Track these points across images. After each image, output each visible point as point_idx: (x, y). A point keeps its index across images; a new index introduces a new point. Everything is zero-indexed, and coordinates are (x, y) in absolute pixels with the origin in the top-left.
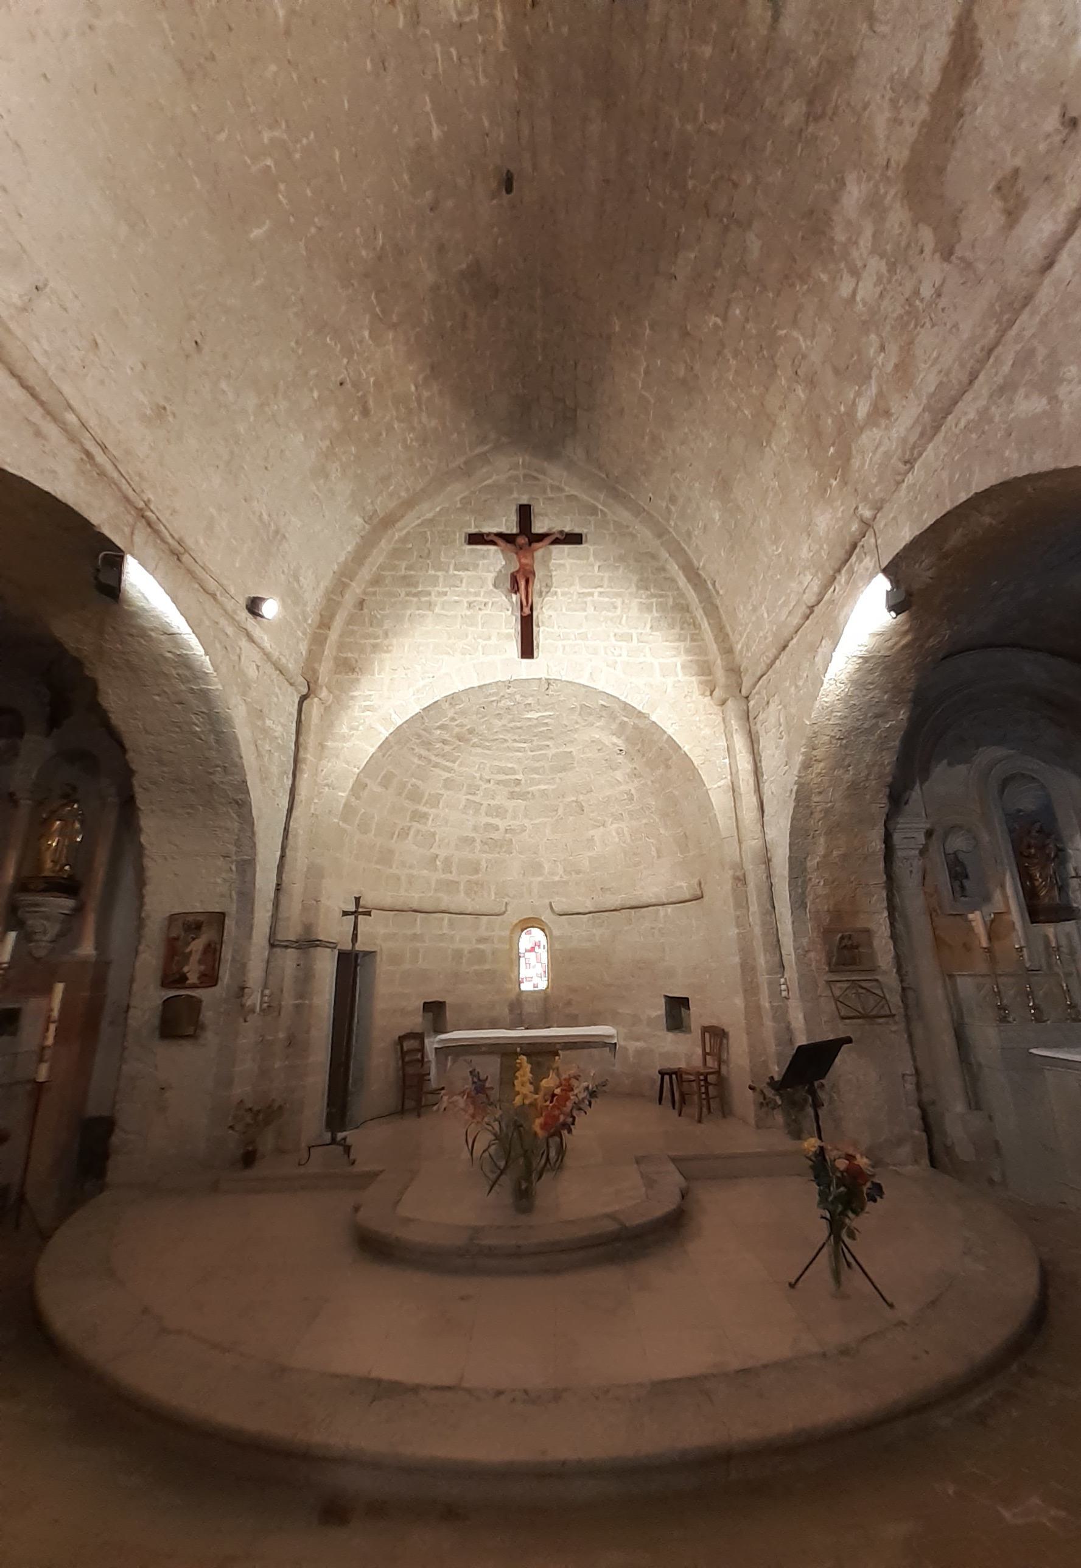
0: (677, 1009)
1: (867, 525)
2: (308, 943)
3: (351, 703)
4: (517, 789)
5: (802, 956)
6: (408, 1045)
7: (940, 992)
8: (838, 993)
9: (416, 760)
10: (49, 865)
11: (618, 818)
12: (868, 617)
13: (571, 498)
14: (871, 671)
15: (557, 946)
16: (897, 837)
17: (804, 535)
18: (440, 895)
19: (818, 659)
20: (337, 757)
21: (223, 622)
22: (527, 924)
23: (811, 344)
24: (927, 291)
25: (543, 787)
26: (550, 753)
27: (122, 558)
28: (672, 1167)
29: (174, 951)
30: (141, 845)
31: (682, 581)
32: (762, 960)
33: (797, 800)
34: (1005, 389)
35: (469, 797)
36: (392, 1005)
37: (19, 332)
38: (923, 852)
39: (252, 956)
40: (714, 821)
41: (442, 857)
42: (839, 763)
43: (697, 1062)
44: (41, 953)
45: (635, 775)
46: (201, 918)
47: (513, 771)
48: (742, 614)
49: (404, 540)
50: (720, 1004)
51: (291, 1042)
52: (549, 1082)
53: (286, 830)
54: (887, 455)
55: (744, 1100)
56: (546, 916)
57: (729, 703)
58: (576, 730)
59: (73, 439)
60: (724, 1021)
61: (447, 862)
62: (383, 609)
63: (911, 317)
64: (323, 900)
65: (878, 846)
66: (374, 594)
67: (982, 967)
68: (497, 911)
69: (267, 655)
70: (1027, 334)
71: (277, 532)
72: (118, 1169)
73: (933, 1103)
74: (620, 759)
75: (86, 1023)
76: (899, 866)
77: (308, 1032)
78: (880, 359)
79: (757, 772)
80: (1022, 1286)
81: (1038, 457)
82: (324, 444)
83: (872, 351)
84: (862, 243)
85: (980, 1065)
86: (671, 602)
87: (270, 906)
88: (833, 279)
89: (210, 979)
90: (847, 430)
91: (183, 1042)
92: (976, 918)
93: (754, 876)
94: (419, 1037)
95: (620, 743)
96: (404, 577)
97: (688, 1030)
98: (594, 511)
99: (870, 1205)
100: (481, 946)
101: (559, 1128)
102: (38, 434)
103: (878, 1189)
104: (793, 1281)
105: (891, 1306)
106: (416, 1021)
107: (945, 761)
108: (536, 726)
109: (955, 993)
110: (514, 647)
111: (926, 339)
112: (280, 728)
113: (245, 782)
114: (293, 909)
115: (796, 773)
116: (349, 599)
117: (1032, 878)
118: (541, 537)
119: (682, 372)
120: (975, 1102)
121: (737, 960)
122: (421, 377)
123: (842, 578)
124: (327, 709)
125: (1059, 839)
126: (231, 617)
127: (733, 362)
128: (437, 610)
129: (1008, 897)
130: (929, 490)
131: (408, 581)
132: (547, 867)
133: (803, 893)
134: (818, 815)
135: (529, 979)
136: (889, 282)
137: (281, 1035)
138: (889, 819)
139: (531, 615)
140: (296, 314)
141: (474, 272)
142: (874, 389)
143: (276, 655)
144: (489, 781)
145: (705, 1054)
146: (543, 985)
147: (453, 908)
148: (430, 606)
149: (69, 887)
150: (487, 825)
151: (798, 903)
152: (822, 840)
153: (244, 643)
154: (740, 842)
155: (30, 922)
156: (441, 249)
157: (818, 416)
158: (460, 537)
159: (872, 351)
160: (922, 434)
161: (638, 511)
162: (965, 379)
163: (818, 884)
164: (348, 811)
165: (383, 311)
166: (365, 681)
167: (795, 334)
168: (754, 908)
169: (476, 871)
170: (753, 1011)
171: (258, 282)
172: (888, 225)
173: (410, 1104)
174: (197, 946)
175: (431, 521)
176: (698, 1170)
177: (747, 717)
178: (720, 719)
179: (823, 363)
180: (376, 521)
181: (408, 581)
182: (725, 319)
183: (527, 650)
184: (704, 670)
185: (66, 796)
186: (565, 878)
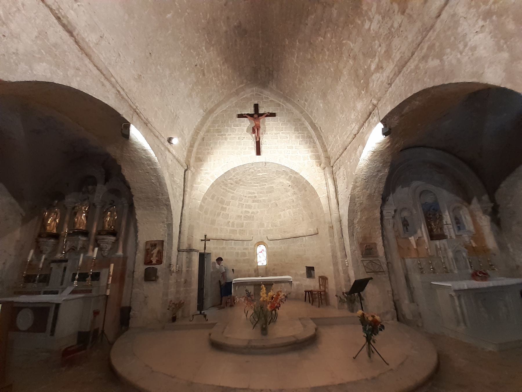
0: (310, 270)
1: (375, 106)
2: (190, 250)
4: (255, 199)
5: (353, 252)
7: (400, 264)
8: (365, 264)
9: (222, 190)
10: (107, 226)
11: (289, 208)
12: (376, 137)
13: (271, 101)
14: (376, 156)
15: (269, 251)
16: (384, 213)
17: (353, 110)
19: (358, 152)
21: (161, 146)
23: (354, 46)
24: (396, 25)
26: (266, 187)
27: (129, 125)
28: (311, 321)
29: (148, 253)
30: (136, 220)
31: (310, 128)
32: (339, 254)
33: (350, 200)
34: (425, 58)
37: (96, 52)
38: (393, 217)
40: (322, 208)
41: (231, 222)
42: (365, 188)
43: (317, 288)
44: (106, 254)
45: (295, 193)
47: (254, 193)
48: (330, 138)
49: (216, 117)
50: (324, 269)
51: (186, 282)
52: (271, 294)
53: (182, 213)
54: (382, 82)
55: (334, 300)
56: (266, 241)
57: (326, 168)
58: (275, 179)
59: (114, 86)
60: (326, 275)
61: (233, 225)
63: (390, 35)
64: (194, 237)
65: (378, 215)
67: (414, 255)
69: (174, 156)
70: (432, 38)
71: (176, 116)
72: (133, 323)
73: (398, 300)
74: (290, 188)
75: (121, 277)
76: (385, 222)
77: (191, 279)
78: (379, 49)
79: (336, 191)
80: (431, 360)
81: (436, 80)
82: (191, 86)
83: (376, 47)
84: (372, 10)
85: (414, 288)
86: (306, 135)
87: (177, 239)
88: (362, 23)
89: (159, 262)
90: (368, 74)
91: (152, 282)
92: (412, 239)
95: (290, 183)
97: (314, 277)
98: (279, 105)
99: (380, 332)
101: (275, 308)
102: (103, 85)
103: (383, 327)
104: (354, 356)
105: (388, 364)
107: (400, 186)
108: (262, 178)
109: (405, 264)
110: (254, 152)
111: (396, 42)
112: (179, 181)
113: (169, 198)
114: (185, 239)
115: (350, 191)
116: (199, 138)
117: (431, 225)
118: (262, 115)
119: (309, 57)
120: (412, 300)
122: (221, 62)
123: (366, 124)
124: (193, 174)
125: (441, 212)
126: (163, 144)
127: (327, 53)
128: (228, 140)
129: (423, 232)
130: (397, 93)
131: (218, 131)
132: (265, 224)
136: (382, 22)
137: (183, 280)
138: (382, 206)
140: (181, 43)
141: (239, 26)
142: (377, 60)
143: (177, 156)
145: (320, 285)
146: (265, 263)
147: (235, 238)
148: (226, 139)
149: (114, 233)
150: (245, 211)
151: (351, 235)
152: (359, 213)
153: (167, 152)
154: (331, 215)
155: (102, 245)
156: (228, 18)
157: (357, 70)
158: (235, 116)
159: (376, 47)
160: (395, 74)
161: (294, 105)
162: (410, 55)
164: (201, 207)
165: (209, 40)
167: (349, 42)
168: (336, 236)
169: (242, 226)
170: (337, 271)
171: (170, 32)
172: (382, 3)
174: (155, 251)
176: (321, 322)
177: (333, 173)
178: (323, 174)
179: (359, 51)
180: (207, 111)
181: (218, 131)
182: (324, 38)
183: (258, 153)
184: (318, 158)
185: (111, 204)
186: (272, 228)
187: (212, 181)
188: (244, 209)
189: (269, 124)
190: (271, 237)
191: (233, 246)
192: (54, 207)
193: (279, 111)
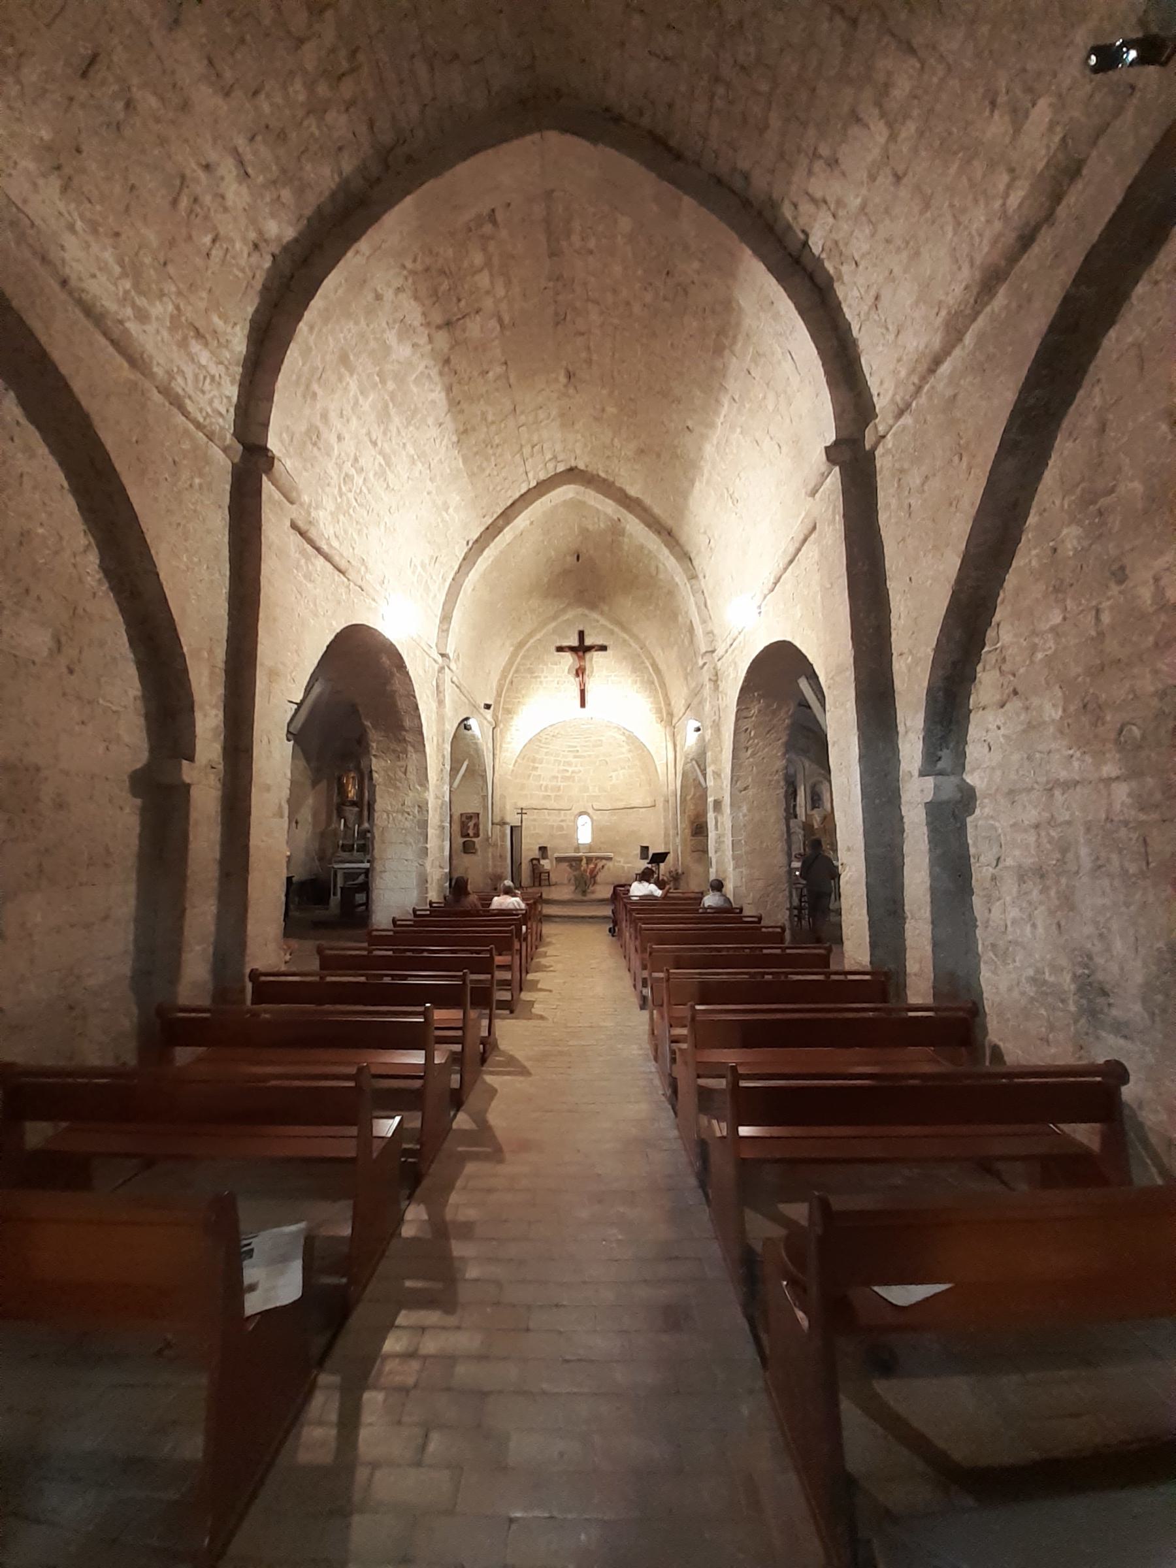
22: (581, 814)
32: (671, 832)
36: (529, 848)
39: (487, 827)
45: (630, 751)
56: (590, 811)
89: (477, 835)
98: (612, 632)
114: (496, 810)
131: (531, 671)
151: (683, 812)
158: (553, 649)
166: (515, 717)
181: (531, 671)
183: (583, 704)
184: (659, 711)
188: (562, 768)
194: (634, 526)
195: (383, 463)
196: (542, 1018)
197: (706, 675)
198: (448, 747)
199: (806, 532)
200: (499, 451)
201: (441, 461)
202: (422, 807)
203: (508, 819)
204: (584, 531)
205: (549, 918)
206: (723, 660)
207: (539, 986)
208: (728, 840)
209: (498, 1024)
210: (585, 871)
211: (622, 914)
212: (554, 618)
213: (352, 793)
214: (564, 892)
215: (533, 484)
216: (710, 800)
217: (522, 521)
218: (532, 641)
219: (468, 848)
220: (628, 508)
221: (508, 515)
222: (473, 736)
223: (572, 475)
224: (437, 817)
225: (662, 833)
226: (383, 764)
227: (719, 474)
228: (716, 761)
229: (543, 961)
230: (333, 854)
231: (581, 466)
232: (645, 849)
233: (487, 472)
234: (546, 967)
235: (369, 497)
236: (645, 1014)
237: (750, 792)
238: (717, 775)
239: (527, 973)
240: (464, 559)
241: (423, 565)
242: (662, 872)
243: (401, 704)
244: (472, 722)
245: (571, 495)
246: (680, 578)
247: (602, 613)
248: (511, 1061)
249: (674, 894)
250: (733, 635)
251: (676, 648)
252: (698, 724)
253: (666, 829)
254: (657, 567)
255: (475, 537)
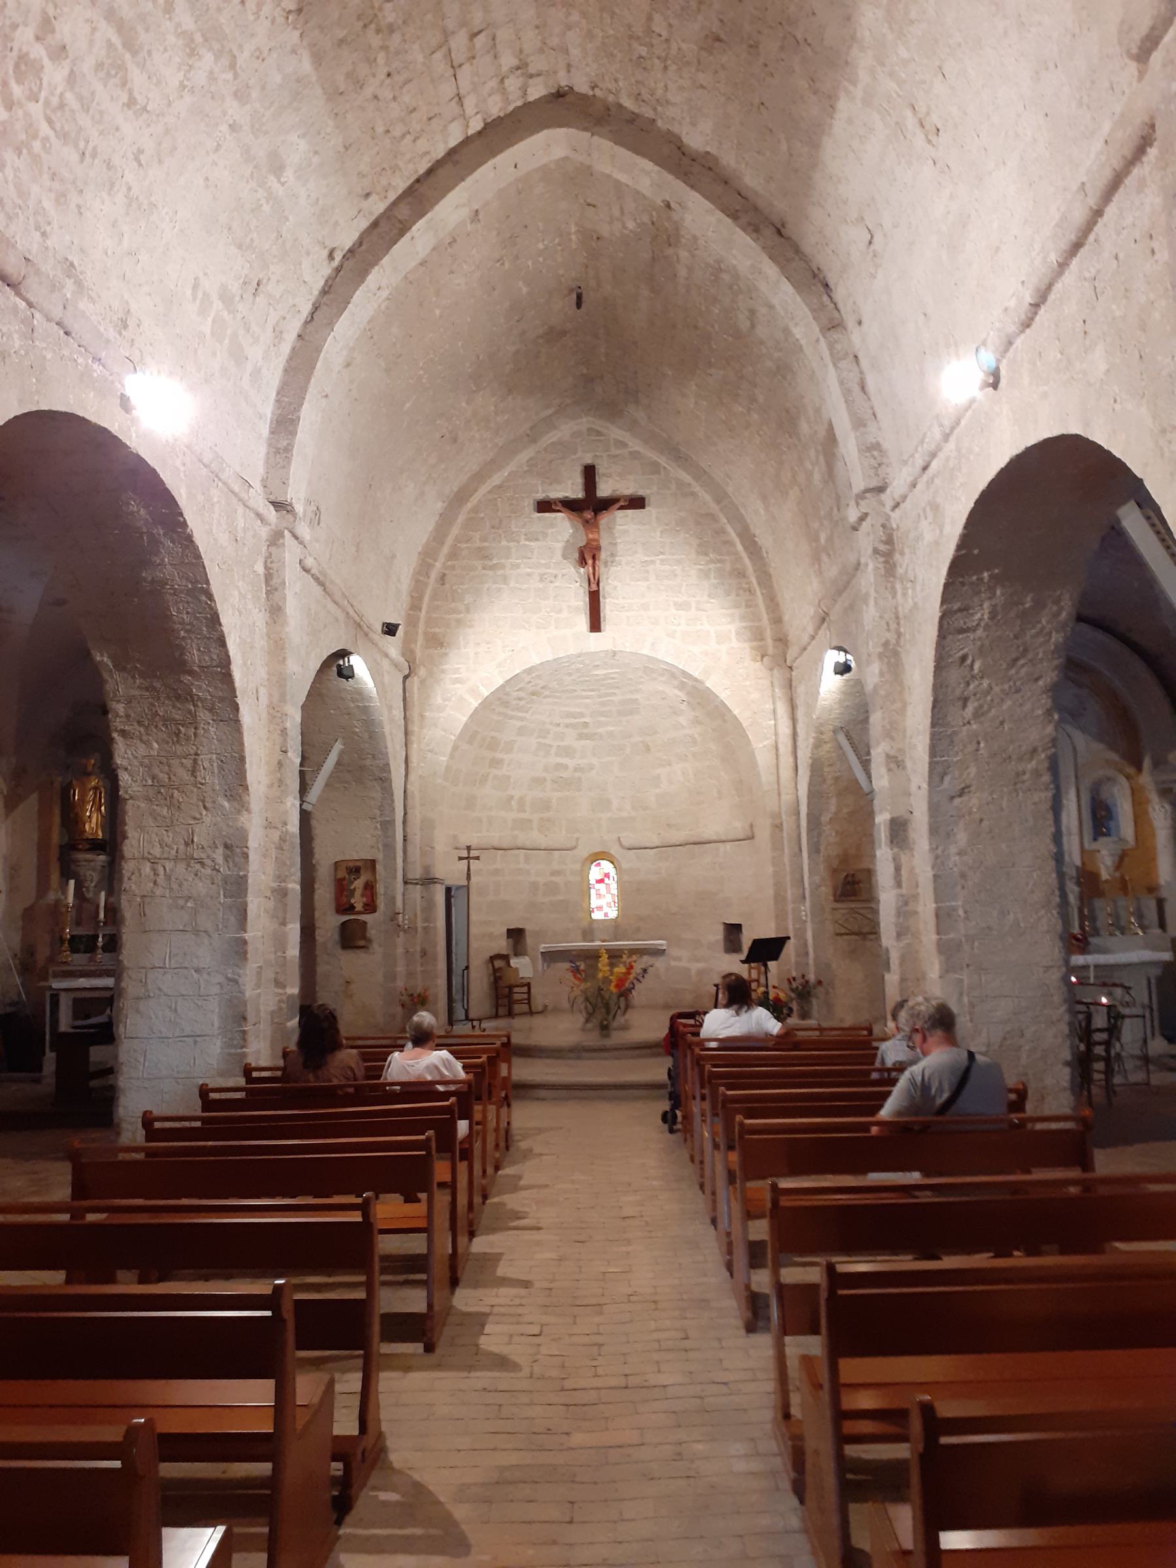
2: (428, 881)
3: (442, 676)
4: (585, 731)
5: (815, 888)
6: (498, 963)
9: (495, 717)
13: (635, 455)
15: (626, 878)
18: (516, 832)
20: (436, 725)
22: (596, 857)
25: (610, 728)
29: (342, 888)
35: (540, 740)
39: (393, 889)
45: (696, 722)
46: (358, 864)
47: (582, 715)
51: (424, 953)
56: (615, 850)
58: (642, 683)
62: (462, 584)
66: (453, 568)
68: (569, 845)
79: (795, 735)
86: (728, 567)
89: (371, 907)
91: (358, 951)
93: (788, 823)
94: (506, 958)
96: (480, 549)
98: (655, 468)
100: (553, 879)
106: (502, 945)
110: (583, 621)
113: (388, 765)
114: (415, 853)
121: (771, 892)
128: (512, 584)
131: (483, 555)
133: (818, 841)
134: (829, 782)
135: (600, 908)
137: (418, 949)
139: (598, 591)
144: (559, 725)
146: (613, 914)
147: (528, 844)
148: (505, 579)
151: (815, 849)
158: (528, 504)
161: (700, 474)
163: (829, 835)
173: (502, 1011)
174: (359, 884)
175: (500, 487)
181: (483, 555)
183: (595, 625)
184: (757, 635)
187: (475, 703)
188: (554, 760)
189: (626, 531)
190: (629, 839)
191: (521, 866)
192: (89, 774)
193: (655, 488)
194: (700, 217)
195: (116, 40)
196: (502, 1363)
197: (866, 540)
198: (295, 716)
199: (1117, 163)
200: (396, 38)
201: (259, 56)
202: (235, 849)
203: (440, 871)
204: (591, 239)
205: (525, 1089)
206: (906, 505)
207: (501, 1271)
208: (926, 907)
209: (388, 1382)
210: (607, 980)
211: (695, 1084)
212: (532, 437)
213: (93, 823)
214: (562, 1028)
215: (476, 125)
216: (882, 819)
217: (451, 210)
218: (483, 489)
219: (352, 937)
220: (685, 175)
221: (420, 195)
222: (360, 694)
223: (562, 106)
224: (270, 868)
225: (770, 892)
226: (142, 750)
227: (892, 74)
228: (893, 731)
229: (511, 1201)
230: (51, 960)
231: (582, 87)
232: (733, 931)
233: (369, 91)
234: (518, 1216)
235: (84, 120)
236: (763, 1343)
237: (973, 801)
238: (896, 762)
239: (472, 1235)
240: (324, 292)
241: (226, 298)
242: (773, 981)
243: (180, 612)
244: (356, 662)
245: (559, 152)
246: (803, 327)
247: (633, 426)
248: (419, 1503)
249: (808, 1026)
250: (928, 446)
251: (794, 493)
252: (841, 657)
253: (779, 886)
254: (752, 312)
255: (348, 244)
